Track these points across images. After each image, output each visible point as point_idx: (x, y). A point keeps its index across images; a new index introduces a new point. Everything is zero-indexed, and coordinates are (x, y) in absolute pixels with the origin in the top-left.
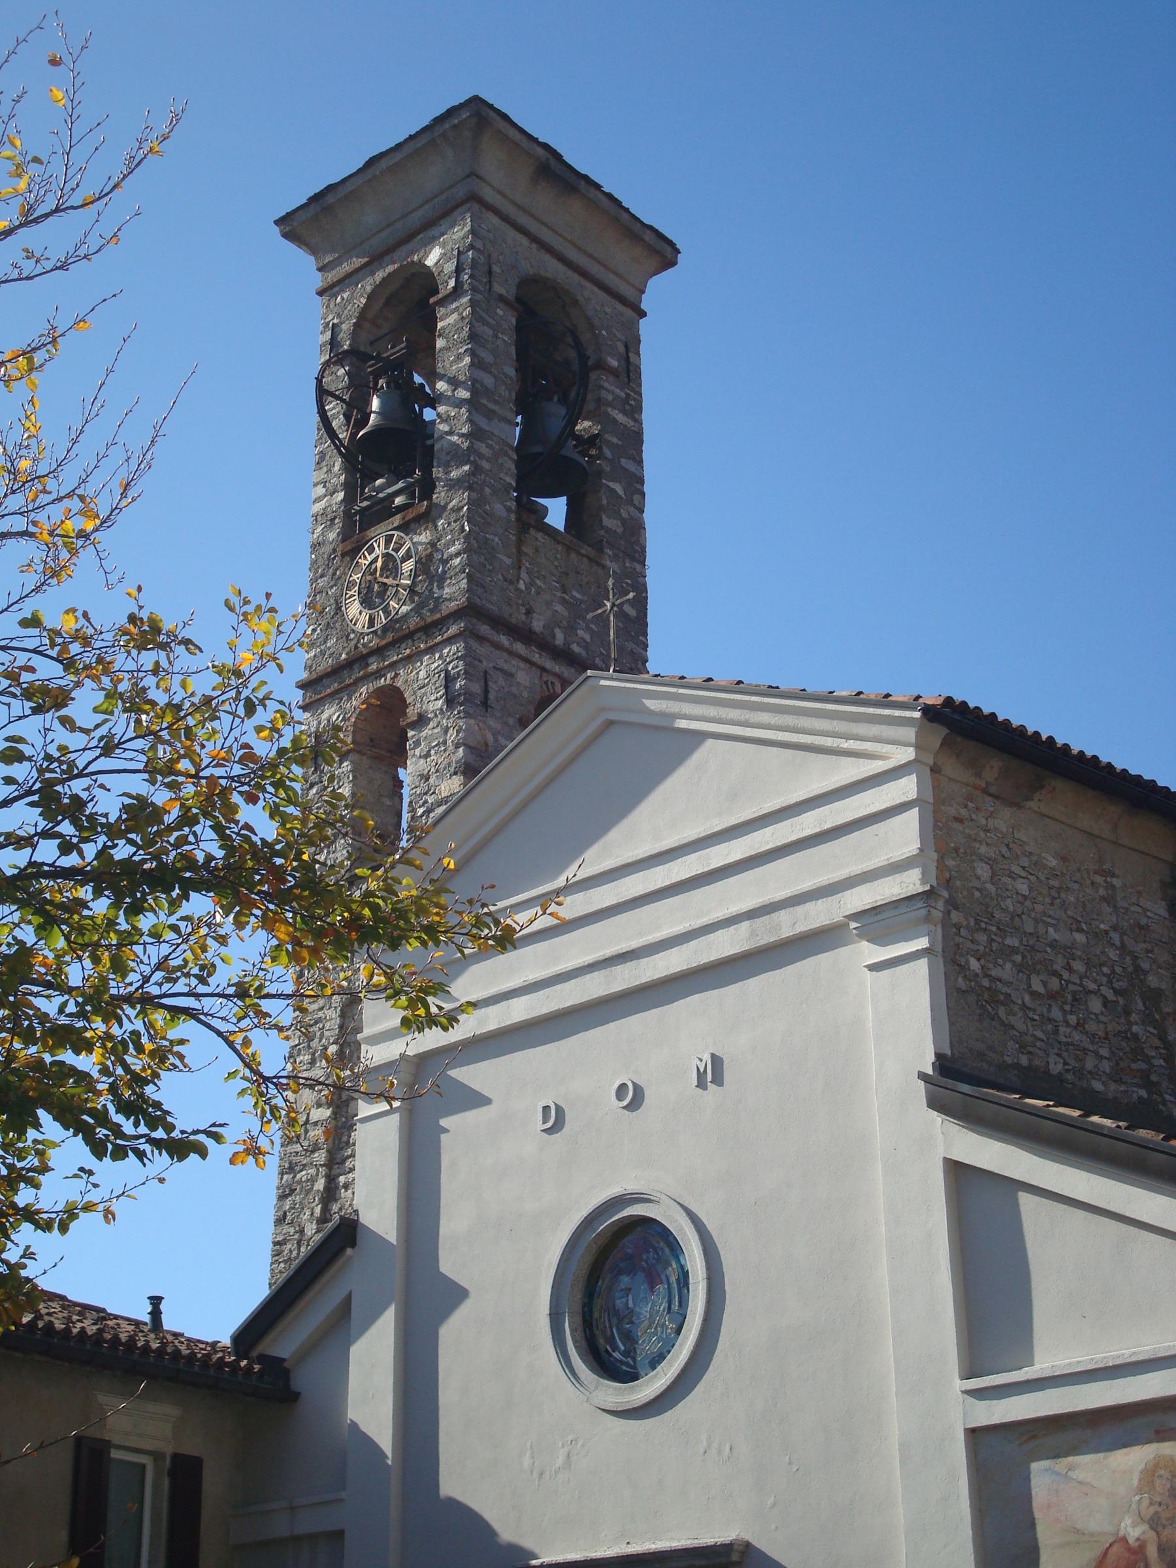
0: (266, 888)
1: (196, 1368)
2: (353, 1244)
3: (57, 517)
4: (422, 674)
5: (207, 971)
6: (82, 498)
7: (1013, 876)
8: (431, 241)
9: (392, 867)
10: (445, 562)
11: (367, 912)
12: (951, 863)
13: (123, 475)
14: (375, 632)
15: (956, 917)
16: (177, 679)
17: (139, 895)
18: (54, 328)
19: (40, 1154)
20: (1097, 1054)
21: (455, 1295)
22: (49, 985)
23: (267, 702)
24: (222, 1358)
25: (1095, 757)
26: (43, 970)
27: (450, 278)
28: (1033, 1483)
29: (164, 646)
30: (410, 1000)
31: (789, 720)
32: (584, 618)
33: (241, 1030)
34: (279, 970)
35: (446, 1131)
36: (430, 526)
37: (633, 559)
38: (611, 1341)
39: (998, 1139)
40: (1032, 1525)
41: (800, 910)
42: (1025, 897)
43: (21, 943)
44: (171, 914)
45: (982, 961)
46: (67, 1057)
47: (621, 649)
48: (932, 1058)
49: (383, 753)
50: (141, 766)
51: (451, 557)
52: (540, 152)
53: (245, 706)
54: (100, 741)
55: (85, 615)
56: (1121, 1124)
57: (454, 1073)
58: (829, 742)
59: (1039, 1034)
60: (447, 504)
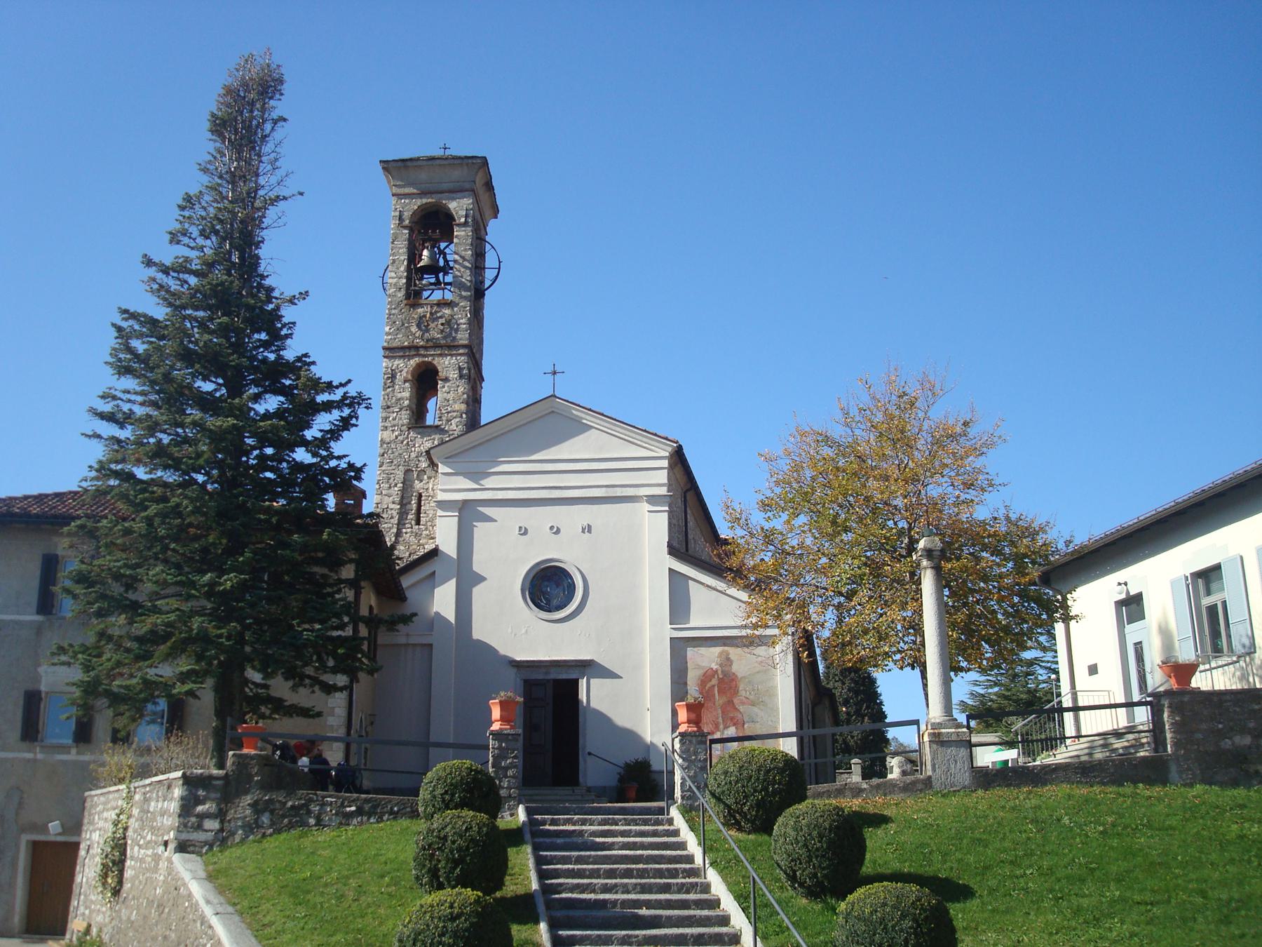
8: (454, 199)
41: (624, 489)
58: (639, 443)
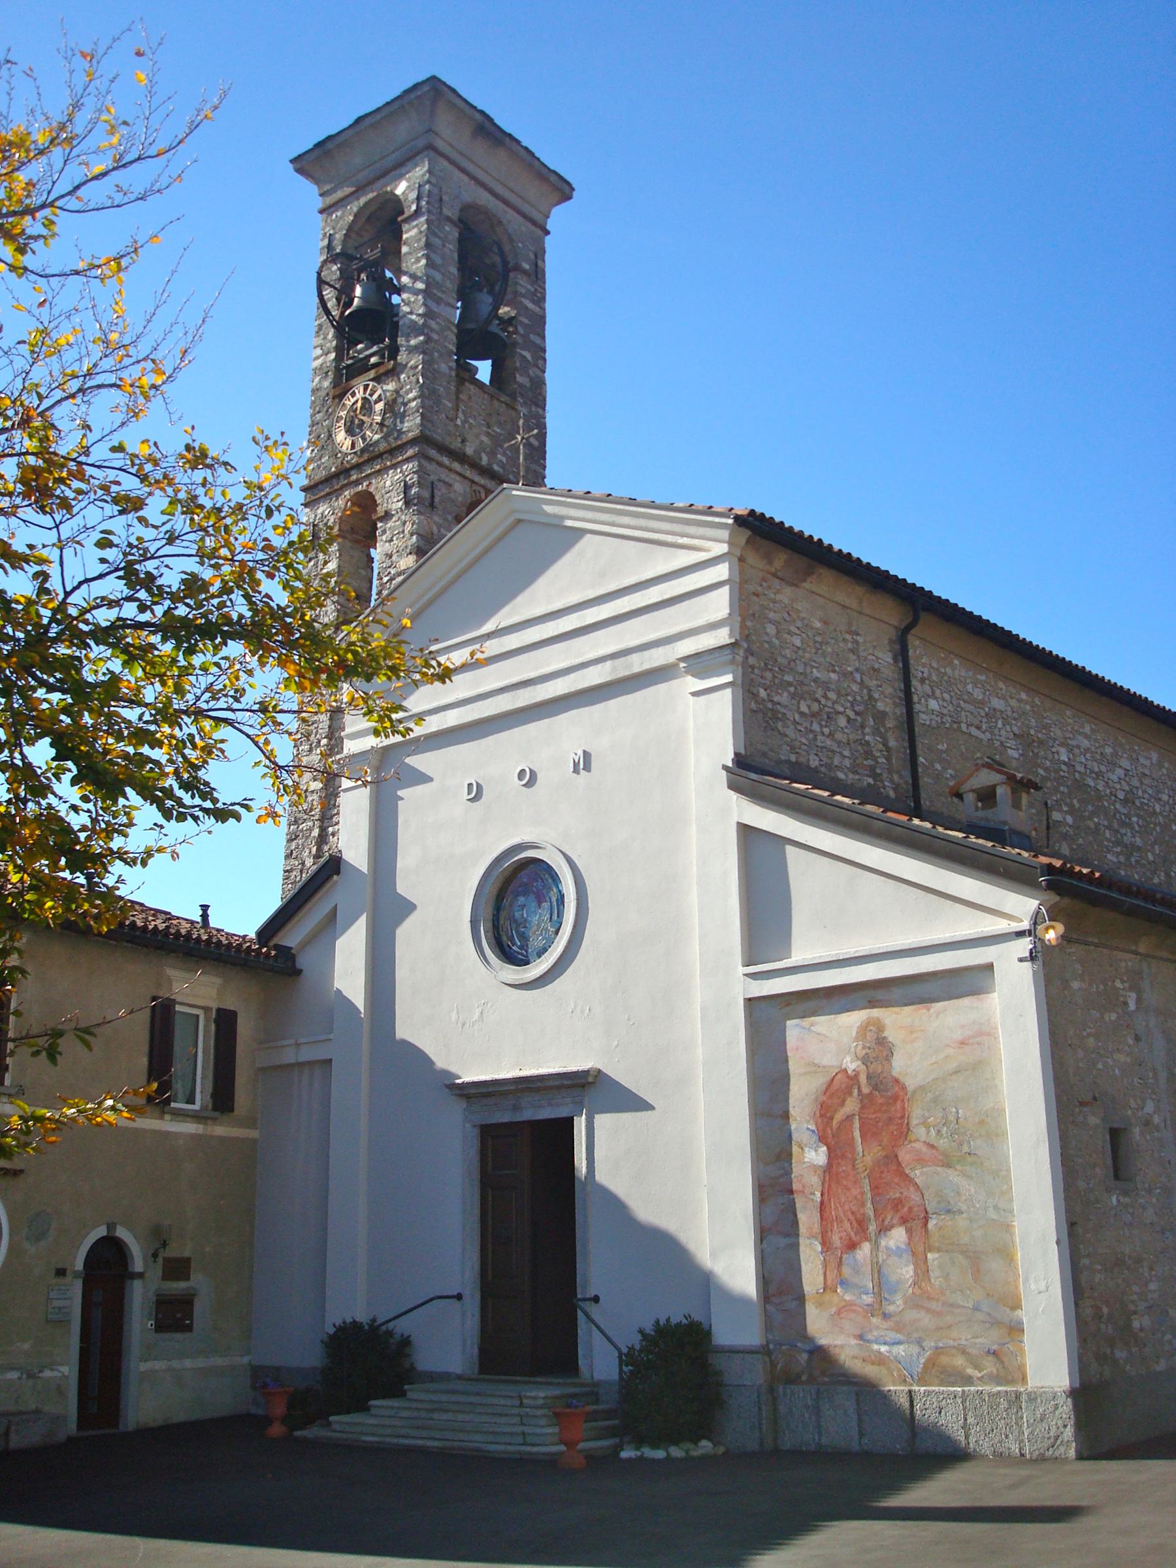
0: (280, 638)
1: (233, 953)
2: (338, 873)
3: (137, 375)
4: (388, 483)
5: (239, 694)
6: (153, 361)
7: (790, 633)
8: (401, 177)
9: (367, 625)
10: (405, 404)
11: (350, 656)
12: (749, 624)
13: (182, 345)
14: (355, 453)
15: (752, 661)
16: (219, 490)
17: (193, 642)
18: (136, 242)
19: (127, 814)
20: (840, 753)
21: (408, 908)
22: (132, 702)
23: (281, 508)
24: (250, 946)
25: (849, 554)
26: (127, 691)
27: (413, 203)
28: (788, 1033)
29: (210, 467)
30: (380, 716)
31: (642, 522)
32: (502, 447)
33: (264, 734)
34: (289, 694)
35: (402, 799)
36: (395, 378)
37: (537, 405)
38: (512, 939)
39: (774, 811)
40: (786, 1061)
41: (647, 654)
42: (799, 648)
43: (112, 673)
44: (214, 655)
45: (768, 691)
46: (146, 750)
47: (527, 469)
48: (732, 756)
49: (360, 538)
50: (194, 552)
51: (410, 401)
52: (478, 116)
53: (266, 511)
54: (165, 534)
55: (155, 444)
56: (856, 801)
57: (408, 760)
58: (670, 538)
59: (804, 741)
60: (407, 363)
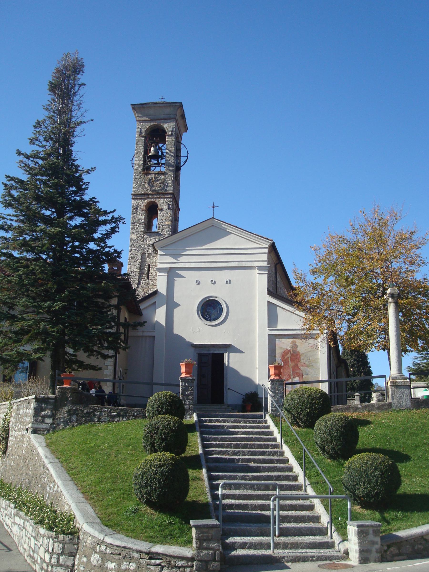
4: (162, 202)
21: (178, 305)
31: (248, 236)
58: (254, 241)
